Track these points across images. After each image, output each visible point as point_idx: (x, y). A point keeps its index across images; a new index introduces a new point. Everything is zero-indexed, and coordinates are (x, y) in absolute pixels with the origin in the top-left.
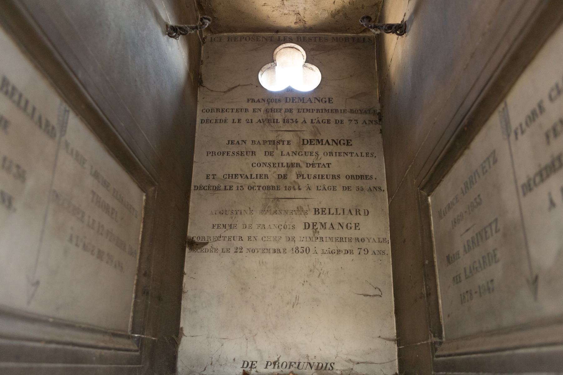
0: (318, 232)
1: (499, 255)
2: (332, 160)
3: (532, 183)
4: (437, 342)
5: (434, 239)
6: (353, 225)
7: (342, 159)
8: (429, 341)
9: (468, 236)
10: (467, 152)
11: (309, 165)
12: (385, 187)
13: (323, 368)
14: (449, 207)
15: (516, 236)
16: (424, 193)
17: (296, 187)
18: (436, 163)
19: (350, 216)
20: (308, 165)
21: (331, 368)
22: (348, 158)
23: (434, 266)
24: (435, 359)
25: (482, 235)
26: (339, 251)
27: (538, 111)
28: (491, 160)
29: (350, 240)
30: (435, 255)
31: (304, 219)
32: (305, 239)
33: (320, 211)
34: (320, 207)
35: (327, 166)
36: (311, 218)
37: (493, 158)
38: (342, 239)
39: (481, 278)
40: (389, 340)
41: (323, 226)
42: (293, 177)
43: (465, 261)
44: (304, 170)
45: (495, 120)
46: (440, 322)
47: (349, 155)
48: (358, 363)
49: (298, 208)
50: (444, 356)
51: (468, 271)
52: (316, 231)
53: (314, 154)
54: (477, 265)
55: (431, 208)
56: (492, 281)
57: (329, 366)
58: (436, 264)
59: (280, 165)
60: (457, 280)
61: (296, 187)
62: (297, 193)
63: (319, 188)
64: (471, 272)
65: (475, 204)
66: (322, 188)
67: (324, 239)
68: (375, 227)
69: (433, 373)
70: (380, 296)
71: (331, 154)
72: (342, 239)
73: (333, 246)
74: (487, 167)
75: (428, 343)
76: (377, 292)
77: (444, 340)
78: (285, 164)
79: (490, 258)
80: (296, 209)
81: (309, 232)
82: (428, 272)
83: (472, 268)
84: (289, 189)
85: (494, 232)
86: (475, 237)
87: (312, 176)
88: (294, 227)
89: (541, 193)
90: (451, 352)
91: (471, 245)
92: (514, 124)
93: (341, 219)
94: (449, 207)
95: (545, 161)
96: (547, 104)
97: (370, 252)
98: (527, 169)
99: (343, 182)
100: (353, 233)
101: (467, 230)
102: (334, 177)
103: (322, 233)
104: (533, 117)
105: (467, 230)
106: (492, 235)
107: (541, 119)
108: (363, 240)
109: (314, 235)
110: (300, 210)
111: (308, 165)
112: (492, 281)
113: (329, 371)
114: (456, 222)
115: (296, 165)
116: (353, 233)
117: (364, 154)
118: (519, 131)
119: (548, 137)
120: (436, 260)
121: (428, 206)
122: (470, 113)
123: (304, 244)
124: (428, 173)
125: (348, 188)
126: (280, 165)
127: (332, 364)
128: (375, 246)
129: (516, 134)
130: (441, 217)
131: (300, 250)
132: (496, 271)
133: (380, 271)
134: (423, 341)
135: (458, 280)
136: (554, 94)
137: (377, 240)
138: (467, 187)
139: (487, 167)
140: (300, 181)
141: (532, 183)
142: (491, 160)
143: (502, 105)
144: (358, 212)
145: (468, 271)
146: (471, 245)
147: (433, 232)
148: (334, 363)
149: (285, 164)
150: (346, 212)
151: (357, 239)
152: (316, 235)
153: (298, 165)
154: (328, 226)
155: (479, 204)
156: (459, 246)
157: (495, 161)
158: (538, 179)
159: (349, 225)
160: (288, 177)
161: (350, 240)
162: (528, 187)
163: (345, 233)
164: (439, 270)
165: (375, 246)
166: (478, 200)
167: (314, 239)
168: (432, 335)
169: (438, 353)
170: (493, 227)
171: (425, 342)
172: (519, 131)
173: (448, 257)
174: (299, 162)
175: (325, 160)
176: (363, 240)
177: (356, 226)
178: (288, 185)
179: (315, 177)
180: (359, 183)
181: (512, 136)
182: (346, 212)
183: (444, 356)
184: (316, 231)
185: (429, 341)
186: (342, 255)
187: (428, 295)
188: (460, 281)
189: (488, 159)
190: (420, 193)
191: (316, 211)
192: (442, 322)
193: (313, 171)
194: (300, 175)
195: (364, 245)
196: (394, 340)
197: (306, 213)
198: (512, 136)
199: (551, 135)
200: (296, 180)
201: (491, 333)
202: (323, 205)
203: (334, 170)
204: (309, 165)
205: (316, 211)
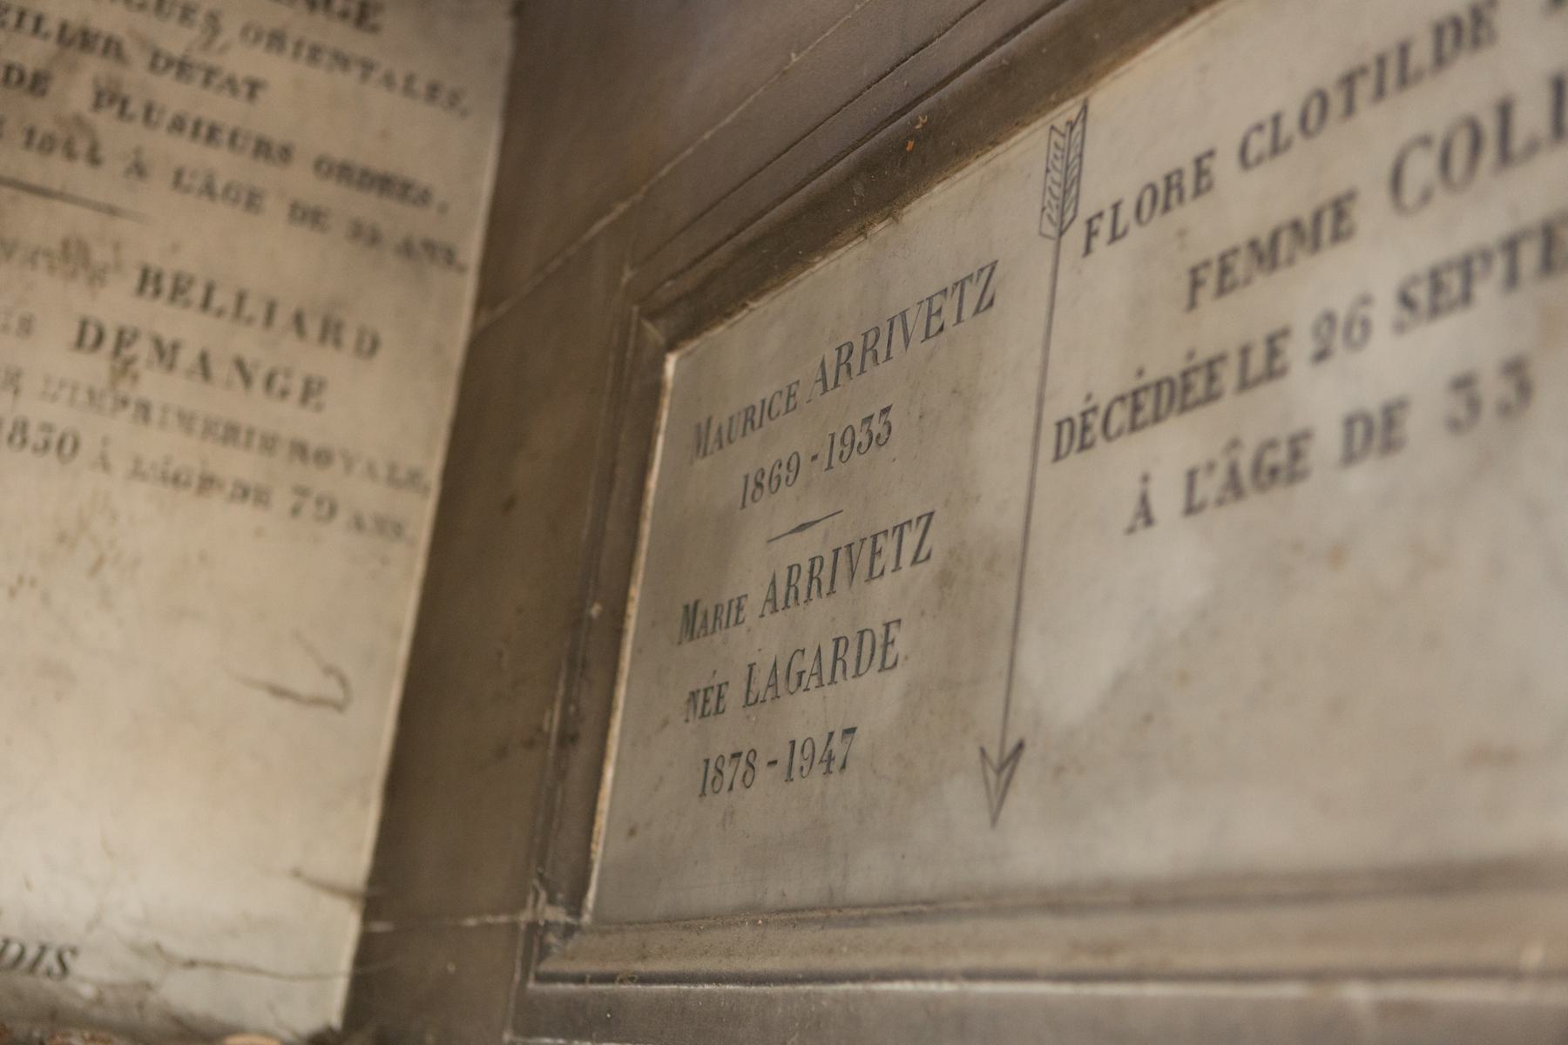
0: (135, 378)
1: (901, 646)
2: (277, 70)
3: (1096, 422)
4: (557, 923)
5: (646, 528)
6: (297, 386)
7: (319, 77)
8: (525, 917)
9: (801, 550)
10: (880, 229)
11: (162, 63)
12: (471, 251)
13: (25, 964)
14: (751, 419)
15: (984, 592)
16: (654, 333)
17: (82, 146)
18: (745, 237)
19: (290, 341)
20: (158, 61)
21: (57, 969)
22: (348, 81)
23: (619, 632)
24: (531, 985)
25: (856, 560)
26: (208, 483)
27: (1189, 183)
28: (972, 294)
29: (269, 444)
30: (635, 592)
31: (79, 300)
32: (65, 394)
33: (167, 284)
34: (169, 266)
35: (244, 90)
36: (116, 304)
37: (980, 289)
38: (232, 434)
39: (807, 715)
40: (333, 889)
41: (166, 353)
42: (75, 93)
43: (760, 640)
44: (136, 77)
45: (1028, 148)
46: (587, 851)
47: (355, 72)
48: (192, 964)
49: (66, 244)
50: (580, 979)
51: (761, 679)
52: (124, 369)
53: (200, 18)
54: (807, 663)
55: (666, 402)
56: (850, 731)
57: (50, 959)
58: (631, 625)
59: (29, 23)
60: (705, 703)
61: (82, 146)
62: (77, 176)
63: (186, 180)
64: (773, 685)
65: (861, 437)
66: (198, 183)
67: (156, 414)
68: (392, 413)
69: (507, 1037)
70: (339, 707)
71: (276, 40)
72: (232, 434)
73: (188, 452)
74: (949, 315)
75: (514, 926)
76: (332, 689)
77: (586, 918)
78: (51, 26)
79: (868, 650)
80: (55, 246)
81: (95, 367)
82: (585, 653)
83: (781, 672)
84: (47, 146)
85: (907, 556)
86: (828, 563)
87: (167, 119)
88: (26, 326)
89: (1123, 463)
90: (610, 967)
91: (802, 586)
92: (1094, 195)
93: (248, 343)
94: (751, 419)
95: (1165, 362)
96: (1225, 168)
97: (343, 516)
98: (1093, 370)
99: (301, 182)
100: (290, 419)
101: (802, 528)
102: (263, 148)
103: (153, 384)
104: (1166, 194)
105: (802, 528)
106: (897, 568)
107: (1189, 213)
108: (323, 457)
109: (113, 383)
110: (73, 257)
111: (158, 61)
112: (850, 731)
113: (48, 983)
114: (760, 484)
115: (101, 44)
116: (290, 419)
117: (420, 86)
118: (1104, 227)
119: (1196, 284)
120: (633, 610)
121: (655, 390)
122: (944, 93)
123: (61, 416)
124: (697, 260)
125: (310, 216)
126: (29, 23)
127: (67, 957)
128: (369, 497)
129: (1091, 234)
130: (700, 447)
131: (35, 436)
132: (876, 701)
133: (372, 608)
134: (495, 913)
135: (711, 705)
136: (1260, 143)
137: (382, 471)
138: (844, 365)
139: (949, 315)
140: (105, 122)
141: (1096, 422)
142: (972, 294)
143: (1070, 109)
144: (331, 331)
145: (761, 679)
146: (802, 586)
147: (650, 501)
148: (74, 952)
149: (51, 26)
150: (283, 317)
151: (300, 450)
152: (124, 387)
153: (113, 48)
154: (187, 358)
155: (876, 441)
156: (751, 576)
157: (986, 304)
158: (1120, 416)
159: (280, 381)
160: (54, 88)
161: (269, 444)
162: (1079, 434)
163: (255, 410)
164: (637, 650)
165: (369, 497)
166: (877, 427)
167: (108, 402)
168: (543, 895)
169: (548, 966)
170: (911, 539)
171: (503, 919)
172: (1104, 227)
173: (690, 612)
174: (120, 33)
175: (242, 60)
176: (323, 457)
177: (311, 390)
178: (45, 125)
179: (178, 125)
180: (367, 206)
181: (1077, 233)
182: (283, 317)
183: (580, 979)
184: (124, 369)
185: (525, 917)
186: (216, 502)
187: (568, 739)
188: (718, 711)
189: (961, 284)
190: (640, 328)
191: (148, 281)
192: (598, 850)
193: (174, 95)
194: (110, 97)
195: (322, 481)
196: (350, 895)
197: (97, 278)
198: (1077, 233)
199: (1211, 278)
200: (89, 115)
201: (794, 915)
202: (186, 262)
203: (272, 117)
204: (162, 63)
205: (148, 281)
